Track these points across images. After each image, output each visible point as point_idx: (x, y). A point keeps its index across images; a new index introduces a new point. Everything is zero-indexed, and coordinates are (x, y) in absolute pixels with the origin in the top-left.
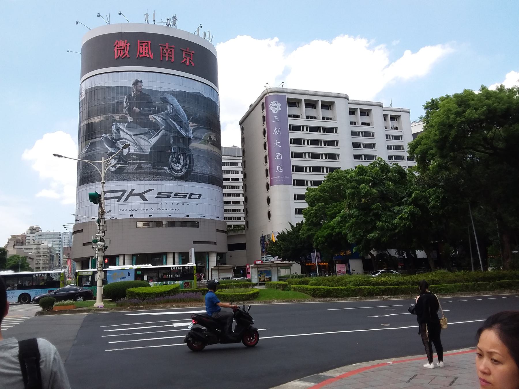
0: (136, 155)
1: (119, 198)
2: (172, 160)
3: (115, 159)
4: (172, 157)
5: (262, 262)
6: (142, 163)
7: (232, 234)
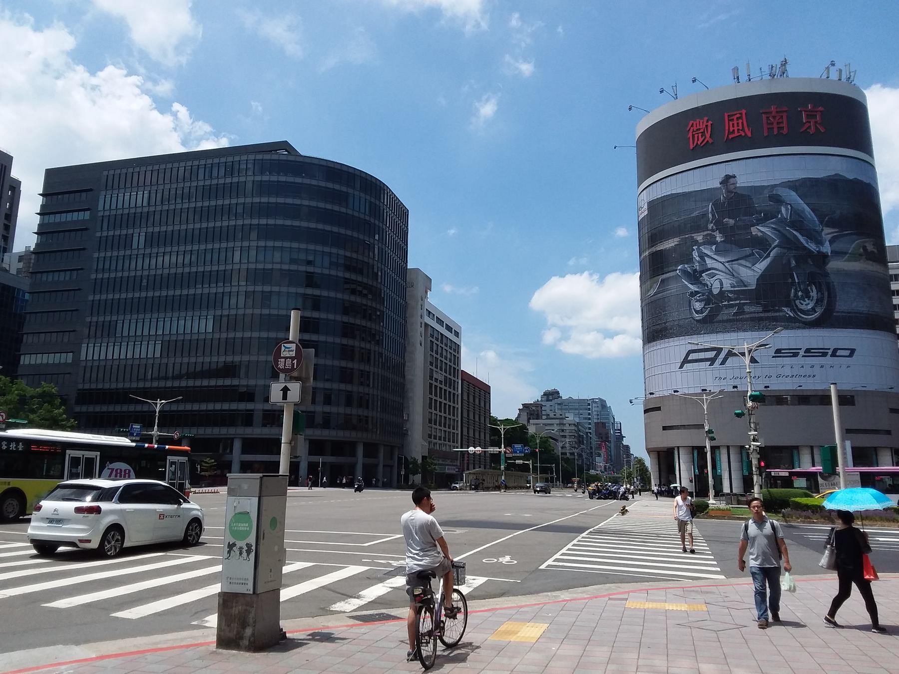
4: (796, 290)
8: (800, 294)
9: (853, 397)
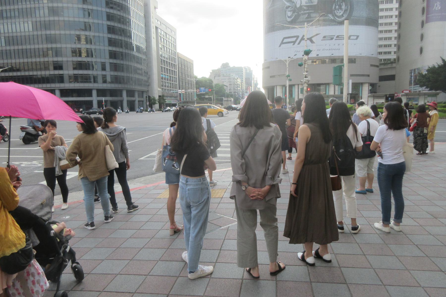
0: (307, 6)
1: (294, 42)
2: (335, 7)
3: (290, 11)
4: (336, 5)
5: (410, 91)
6: (311, 13)
7: (382, 67)
8: (337, 7)
9: (355, 59)
